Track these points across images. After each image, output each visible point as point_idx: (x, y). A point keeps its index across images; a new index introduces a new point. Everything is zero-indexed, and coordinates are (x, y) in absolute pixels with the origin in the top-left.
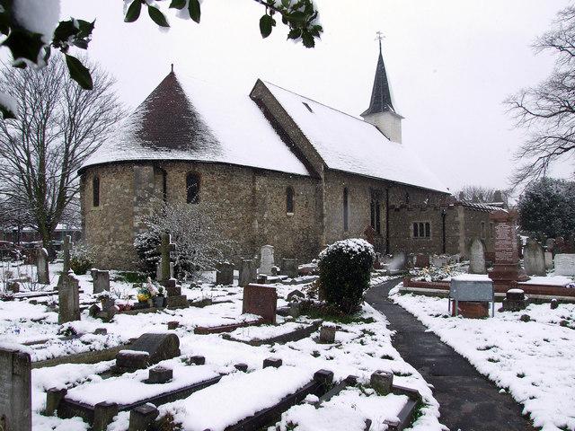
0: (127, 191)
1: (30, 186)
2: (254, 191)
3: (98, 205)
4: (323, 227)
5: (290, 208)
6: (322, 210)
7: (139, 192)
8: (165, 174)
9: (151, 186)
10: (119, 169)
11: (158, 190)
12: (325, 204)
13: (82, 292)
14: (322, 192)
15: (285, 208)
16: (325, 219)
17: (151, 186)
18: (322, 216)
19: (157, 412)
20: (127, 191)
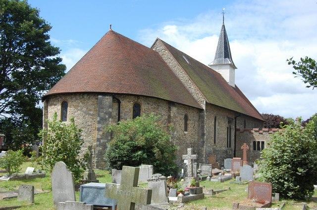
0: (92, 112)
1: (286, 152)
2: (169, 116)
3: (150, 203)
4: (204, 142)
5: (186, 130)
6: (203, 131)
7: (102, 114)
8: (119, 102)
9: (110, 110)
10: (127, 96)
11: (115, 113)
12: (205, 126)
13: (301, 59)
14: (204, 118)
15: (183, 129)
16: (205, 137)
17: (110, 110)
18: (203, 135)
19: (24, 70)
20: (92, 112)
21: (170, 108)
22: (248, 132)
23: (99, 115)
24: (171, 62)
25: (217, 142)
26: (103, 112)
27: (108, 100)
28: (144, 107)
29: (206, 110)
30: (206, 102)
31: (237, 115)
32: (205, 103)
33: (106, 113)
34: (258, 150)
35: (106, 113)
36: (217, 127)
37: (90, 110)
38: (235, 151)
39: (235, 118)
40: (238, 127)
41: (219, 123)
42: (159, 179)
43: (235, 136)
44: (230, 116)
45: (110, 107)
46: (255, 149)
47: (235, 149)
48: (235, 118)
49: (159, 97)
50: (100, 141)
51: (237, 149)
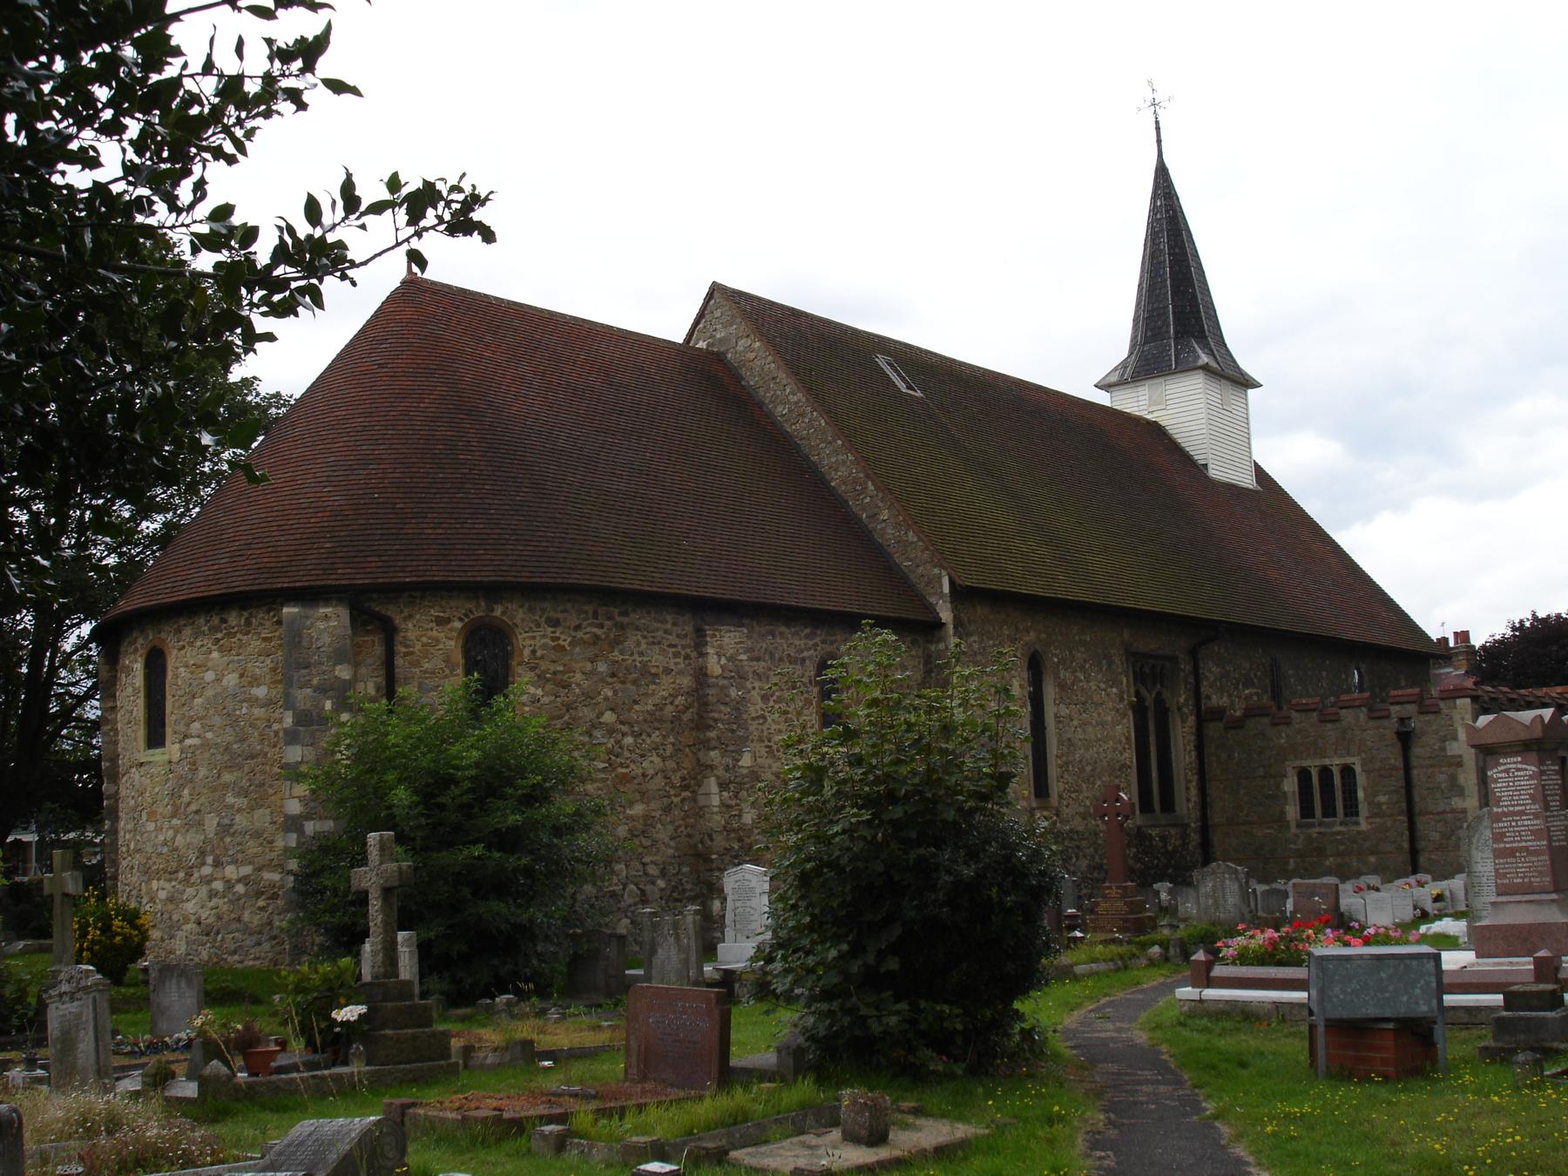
0: (261, 692)
7: (303, 696)
8: (389, 632)
9: (343, 672)
17: (343, 672)
21: (700, 632)
22: (1266, 720)
23: (288, 703)
24: (786, 399)
25: (1055, 787)
26: (307, 684)
27: (328, 623)
28: (532, 637)
29: (958, 623)
30: (952, 583)
31: (1203, 633)
32: (946, 589)
33: (322, 690)
34: (1325, 815)
35: (322, 690)
36: (1050, 710)
37: (256, 681)
38: (1205, 830)
39: (1193, 654)
40: (1217, 700)
41: (1062, 686)
42: (1214, 1067)
43: (1200, 748)
44: (1149, 643)
45: (339, 657)
46: (1306, 810)
47: (1204, 818)
48: (1193, 654)
49: (619, 582)
50: (300, 830)
51: (1217, 818)
